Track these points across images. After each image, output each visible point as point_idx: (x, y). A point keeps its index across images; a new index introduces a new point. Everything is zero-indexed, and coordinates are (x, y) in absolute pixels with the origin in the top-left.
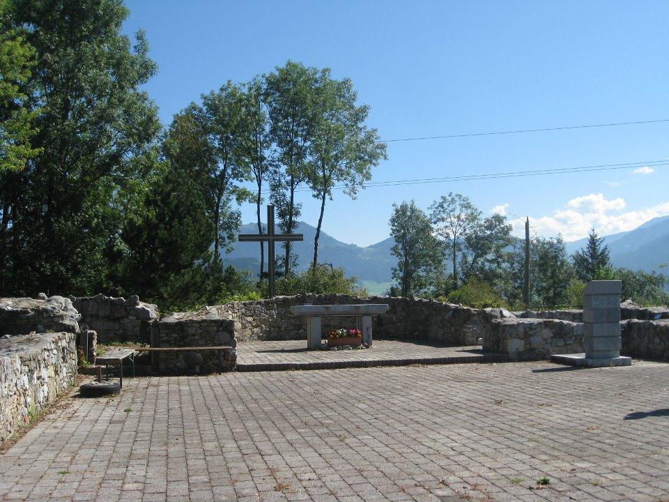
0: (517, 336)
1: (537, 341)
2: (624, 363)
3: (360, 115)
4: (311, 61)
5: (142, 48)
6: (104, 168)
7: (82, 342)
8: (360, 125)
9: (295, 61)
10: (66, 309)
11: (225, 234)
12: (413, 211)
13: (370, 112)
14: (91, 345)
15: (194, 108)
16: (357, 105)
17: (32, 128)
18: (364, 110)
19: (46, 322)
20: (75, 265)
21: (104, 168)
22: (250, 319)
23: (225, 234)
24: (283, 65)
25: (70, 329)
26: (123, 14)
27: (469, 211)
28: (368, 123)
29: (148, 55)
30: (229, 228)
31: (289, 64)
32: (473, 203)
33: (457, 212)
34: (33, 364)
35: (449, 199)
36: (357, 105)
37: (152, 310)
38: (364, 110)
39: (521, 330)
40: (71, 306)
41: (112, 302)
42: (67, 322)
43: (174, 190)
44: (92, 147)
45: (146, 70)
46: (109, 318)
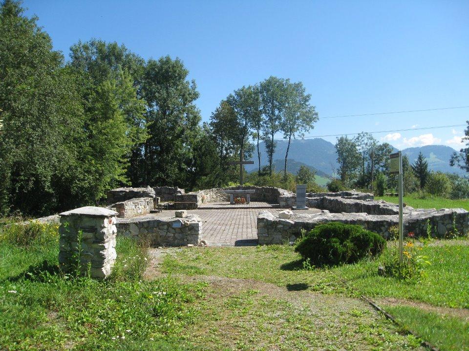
0: (283, 201)
1: (290, 203)
2: (307, 209)
3: (306, 99)
4: (280, 75)
5: (194, 88)
6: (179, 136)
7: (155, 200)
8: (307, 103)
9: (274, 76)
10: (151, 191)
11: (247, 154)
12: (346, 140)
13: (311, 97)
14: (158, 201)
15: (231, 97)
16: (305, 94)
17: (148, 129)
18: (308, 96)
19: (145, 194)
20: (167, 174)
21: (179, 136)
22: (219, 194)
23: (247, 154)
24: (268, 78)
25: (151, 197)
26: (186, 73)
27: (372, 141)
28: (311, 103)
29: (196, 90)
30: (249, 151)
31: (271, 77)
32: (374, 136)
33: (366, 142)
34: (136, 204)
35: (362, 135)
36: (305, 94)
37: (183, 191)
38: (308, 96)
39: (285, 199)
40: (153, 190)
41: (170, 189)
42: (151, 195)
43: (203, 145)
44: (173, 129)
45: (196, 96)
46: (169, 194)
